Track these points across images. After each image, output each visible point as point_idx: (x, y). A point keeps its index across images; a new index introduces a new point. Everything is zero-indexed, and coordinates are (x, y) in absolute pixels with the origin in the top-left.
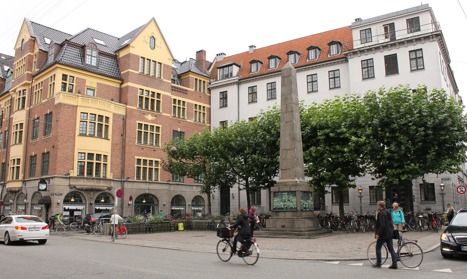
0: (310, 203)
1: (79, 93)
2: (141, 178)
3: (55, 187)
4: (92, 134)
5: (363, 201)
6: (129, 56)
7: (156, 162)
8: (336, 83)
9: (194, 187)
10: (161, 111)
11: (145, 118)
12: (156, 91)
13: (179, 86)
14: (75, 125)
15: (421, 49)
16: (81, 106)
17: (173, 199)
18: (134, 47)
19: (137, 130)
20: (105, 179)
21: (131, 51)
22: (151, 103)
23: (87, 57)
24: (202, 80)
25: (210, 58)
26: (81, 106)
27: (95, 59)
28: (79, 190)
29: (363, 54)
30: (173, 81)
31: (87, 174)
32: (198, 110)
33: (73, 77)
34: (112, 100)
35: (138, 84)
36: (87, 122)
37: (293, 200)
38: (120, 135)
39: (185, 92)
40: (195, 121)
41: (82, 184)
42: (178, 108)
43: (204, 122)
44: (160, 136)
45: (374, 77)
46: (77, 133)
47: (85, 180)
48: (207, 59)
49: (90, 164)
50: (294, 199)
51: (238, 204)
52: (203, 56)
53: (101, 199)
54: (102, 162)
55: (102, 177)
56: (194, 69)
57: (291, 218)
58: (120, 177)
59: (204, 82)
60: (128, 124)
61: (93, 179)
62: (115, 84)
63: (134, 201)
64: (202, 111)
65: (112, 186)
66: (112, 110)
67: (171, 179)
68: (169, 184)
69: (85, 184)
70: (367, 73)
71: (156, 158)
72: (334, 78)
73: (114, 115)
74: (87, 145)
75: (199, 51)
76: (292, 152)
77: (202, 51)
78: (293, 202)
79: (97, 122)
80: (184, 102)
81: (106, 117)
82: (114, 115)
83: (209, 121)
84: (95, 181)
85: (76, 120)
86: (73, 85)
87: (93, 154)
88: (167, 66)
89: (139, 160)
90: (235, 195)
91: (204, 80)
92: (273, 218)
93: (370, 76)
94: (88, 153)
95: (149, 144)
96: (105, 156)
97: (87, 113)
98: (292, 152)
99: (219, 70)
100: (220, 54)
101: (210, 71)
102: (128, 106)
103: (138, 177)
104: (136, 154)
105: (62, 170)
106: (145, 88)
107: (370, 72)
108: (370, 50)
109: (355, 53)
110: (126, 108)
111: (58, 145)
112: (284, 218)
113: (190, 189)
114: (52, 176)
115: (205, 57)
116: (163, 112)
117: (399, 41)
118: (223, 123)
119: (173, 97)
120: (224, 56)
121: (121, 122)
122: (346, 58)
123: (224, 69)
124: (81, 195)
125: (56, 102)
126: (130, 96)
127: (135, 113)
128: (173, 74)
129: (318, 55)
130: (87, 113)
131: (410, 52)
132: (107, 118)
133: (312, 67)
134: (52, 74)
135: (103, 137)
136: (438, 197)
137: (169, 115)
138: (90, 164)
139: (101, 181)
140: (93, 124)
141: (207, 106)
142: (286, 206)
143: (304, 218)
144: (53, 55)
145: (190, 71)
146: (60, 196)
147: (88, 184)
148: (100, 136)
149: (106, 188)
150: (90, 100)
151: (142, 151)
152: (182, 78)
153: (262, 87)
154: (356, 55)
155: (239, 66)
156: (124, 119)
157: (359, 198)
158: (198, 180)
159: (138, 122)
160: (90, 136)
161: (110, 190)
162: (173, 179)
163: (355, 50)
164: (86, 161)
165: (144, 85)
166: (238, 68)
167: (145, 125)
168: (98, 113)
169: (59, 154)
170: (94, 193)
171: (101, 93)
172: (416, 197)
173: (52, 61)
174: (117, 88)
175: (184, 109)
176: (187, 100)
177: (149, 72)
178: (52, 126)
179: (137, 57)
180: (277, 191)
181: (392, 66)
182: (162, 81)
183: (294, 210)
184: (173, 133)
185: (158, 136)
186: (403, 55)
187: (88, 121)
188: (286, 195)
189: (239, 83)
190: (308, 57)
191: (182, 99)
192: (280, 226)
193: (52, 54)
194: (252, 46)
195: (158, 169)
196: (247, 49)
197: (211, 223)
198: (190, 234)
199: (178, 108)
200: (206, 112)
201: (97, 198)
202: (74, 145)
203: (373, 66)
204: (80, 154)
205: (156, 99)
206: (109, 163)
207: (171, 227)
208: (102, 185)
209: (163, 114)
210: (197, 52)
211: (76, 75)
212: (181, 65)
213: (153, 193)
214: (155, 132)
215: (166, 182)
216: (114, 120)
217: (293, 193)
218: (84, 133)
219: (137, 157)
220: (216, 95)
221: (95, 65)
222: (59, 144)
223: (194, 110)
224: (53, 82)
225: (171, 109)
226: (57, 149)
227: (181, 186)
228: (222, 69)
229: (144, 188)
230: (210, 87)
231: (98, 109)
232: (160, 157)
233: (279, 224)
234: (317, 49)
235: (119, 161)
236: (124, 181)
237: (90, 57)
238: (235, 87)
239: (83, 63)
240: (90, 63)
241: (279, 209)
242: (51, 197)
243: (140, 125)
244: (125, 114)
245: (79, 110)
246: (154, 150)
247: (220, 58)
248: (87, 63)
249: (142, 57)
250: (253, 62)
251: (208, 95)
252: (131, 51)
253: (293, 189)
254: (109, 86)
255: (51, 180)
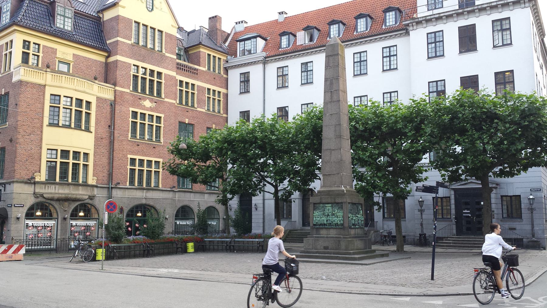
0: (361, 217)
1: (48, 67)
2: (136, 184)
3: (14, 195)
4: (67, 123)
5: (424, 216)
6: (117, 18)
7: (157, 163)
8: (392, 63)
9: (206, 195)
10: (163, 96)
11: (141, 105)
12: (156, 69)
13: (186, 63)
14: (43, 111)
15: (509, 18)
16: (50, 86)
17: (178, 212)
18: (124, 7)
19: (131, 120)
20: (85, 184)
21: (119, 11)
22: (149, 85)
23: (59, 17)
24: (218, 56)
25: (227, 27)
26: (50, 86)
27: (70, 20)
28: (48, 199)
29: (430, 24)
30: (179, 56)
31: (72, 179)
32: (211, 96)
33: (39, 45)
34: (95, 79)
35: (131, 58)
36: (59, 107)
37: (339, 214)
38: (107, 127)
39: (194, 73)
40: (208, 110)
41: (53, 191)
42: (186, 95)
43: (219, 112)
44: (162, 129)
45: (443, 55)
46: (46, 121)
47: (57, 186)
48: (223, 29)
49: (64, 165)
50: (340, 214)
51: (262, 217)
52: (218, 25)
53: (80, 212)
54: (81, 162)
55: (81, 181)
56: (205, 41)
57: (336, 237)
58: (106, 182)
59: (219, 59)
60: (117, 111)
61: (69, 184)
62: (98, 57)
63: (125, 215)
64: (217, 98)
65: (95, 194)
66: (94, 92)
67: (176, 184)
68: (173, 191)
69: (57, 192)
70: (434, 50)
71: (156, 157)
72: (390, 56)
73: (99, 99)
74: (59, 139)
75: (213, 17)
76: (338, 150)
77: (216, 16)
78: (338, 217)
79: (74, 108)
80: (193, 85)
81: (86, 101)
82: (99, 99)
83: (225, 111)
84: (72, 187)
85: (43, 104)
86: (38, 56)
87: (68, 152)
88: (169, 36)
89: (133, 161)
90: (258, 206)
91: (220, 57)
92: (313, 237)
93: (438, 54)
94: (61, 150)
95: (138, 138)
96: (86, 155)
97: (60, 96)
98: (338, 150)
99: (238, 43)
100: (239, 23)
101: (227, 44)
102: (117, 88)
103: (132, 182)
104: (128, 153)
105: (25, 172)
106: (140, 64)
107: (438, 49)
108: (439, 18)
109: (419, 23)
110: (115, 91)
111: (17, 138)
112: (327, 237)
113: (201, 199)
114: (9, 181)
115: (220, 26)
116: (166, 97)
117: (480, 7)
118: (245, 115)
119: (179, 78)
120: (245, 25)
121: (108, 109)
122: (407, 30)
123: (246, 42)
124: (50, 206)
125: (15, 79)
126: (119, 73)
127: (128, 97)
128: (178, 47)
129: (369, 25)
130: (60, 96)
131: (493, 21)
132: (88, 103)
133: (361, 42)
134: (8, 39)
135: (83, 128)
136: (525, 214)
137: (174, 102)
138: (64, 165)
139: (80, 187)
140: (68, 111)
141: (223, 91)
142: (329, 222)
143: (353, 237)
144: (9, 13)
145: (200, 43)
146: (20, 208)
147: (61, 191)
148: (78, 127)
149: (87, 197)
150: (64, 78)
151: (137, 148)
152: (190, 53)
153: (294, 66)
154: (420, 26)
155: (265, 40)
156: (111, 105)
157: (420, 213)
158: (211, 186)
159: (131, 109)
160: (64, 126)
161: (91, 199)
162: (179, 185)
163: (420, 19)
164: (59, 160)
165: (139, 60)
166: (264, 42)
167: (141, 113)
168: (76, 95)
169: (20, 151)
170: (69, 204)
171: (78, 70)
172: (496, 212)
173: (8, 20)
174: (101, 62)
175: (193, 94)
176: (197, 83)
177: (146, 42)
178: (10, 112)
179: (129, 21)
180: (319, 202)
181: (468, 40)
182: (164, 55)
183: (340, 227)
184: (180, 125)
185: (158, 128)
186: (483, 25)
187: (61, 106)
188: (330, 208)
189: (265, 61)
190: (356, 28)
191: (191, 81)
192: (322, 247)
193: (7, 11)
194: (282, 13)
195: (159, 172)
196: (275, 17)
197: (230, 242)
198: (204, 258)
199: (186, 95)
200: (222, 99)
201: (73, 211)
202: (41, 139)
203: (443, 41)
204: (49, 152)
205: (156, 79)
206: (91, 163)
207: (177, 248)
208: (81, 193)
209: (166, 100)
210: (210, 18)
211: (42, 43)
212: (188, 35)
213: (151, 203)
214: (155, 124)
215: (169, 189)
216: (98, 106)
217: (340, 205)
218: (56, 122)
219: (130, 156)
220: (234, 77)
221: (69, 29)
222: (20, 137)
223: (207, 95)
224: (9, 51)
225: (176, 94)
226: (17, 143)
227: (189, 194)
228: (243, 42)
229: (141, 196)
230: (227, 65)
231: (76, 90)
232: (161, 157)
233: (321, 244)
234: (368, 18)
235: (105, 160)
236: (112, 188)
237: (62, 18)
238: (261, 66)
239: (52, 26)
240: (62, 26)
241: (321, 225)
242: (8, 209)
243: (135, 114)
244: (113, 99)
245: (49, 91)
246: (154, 148)
247: (240, 28)
248: (58, 25)
249: (135, 22)
250: (283, 34)
251: (225, 76)
252: (119, 11)
253: (339, 200)
254: (90, 59)
255: (7, 186)
